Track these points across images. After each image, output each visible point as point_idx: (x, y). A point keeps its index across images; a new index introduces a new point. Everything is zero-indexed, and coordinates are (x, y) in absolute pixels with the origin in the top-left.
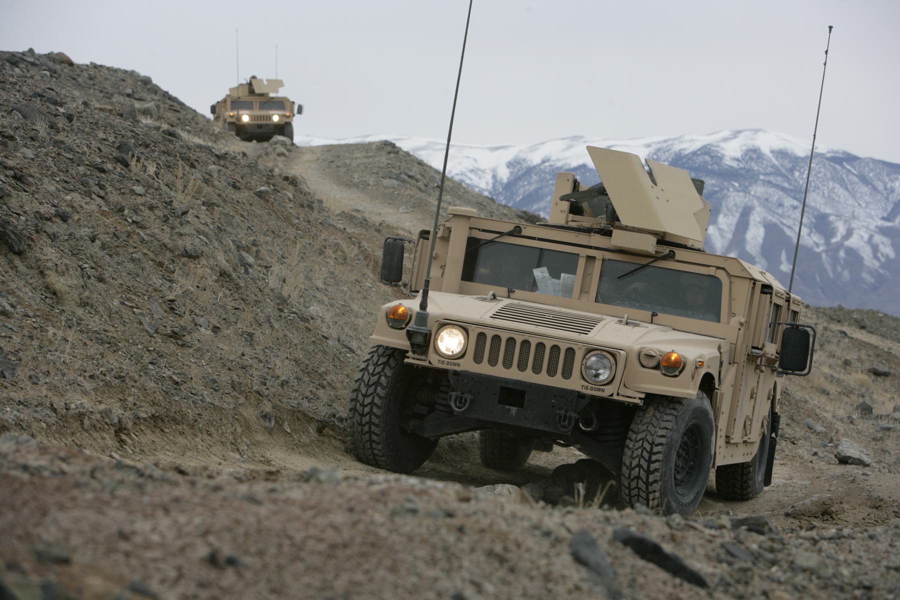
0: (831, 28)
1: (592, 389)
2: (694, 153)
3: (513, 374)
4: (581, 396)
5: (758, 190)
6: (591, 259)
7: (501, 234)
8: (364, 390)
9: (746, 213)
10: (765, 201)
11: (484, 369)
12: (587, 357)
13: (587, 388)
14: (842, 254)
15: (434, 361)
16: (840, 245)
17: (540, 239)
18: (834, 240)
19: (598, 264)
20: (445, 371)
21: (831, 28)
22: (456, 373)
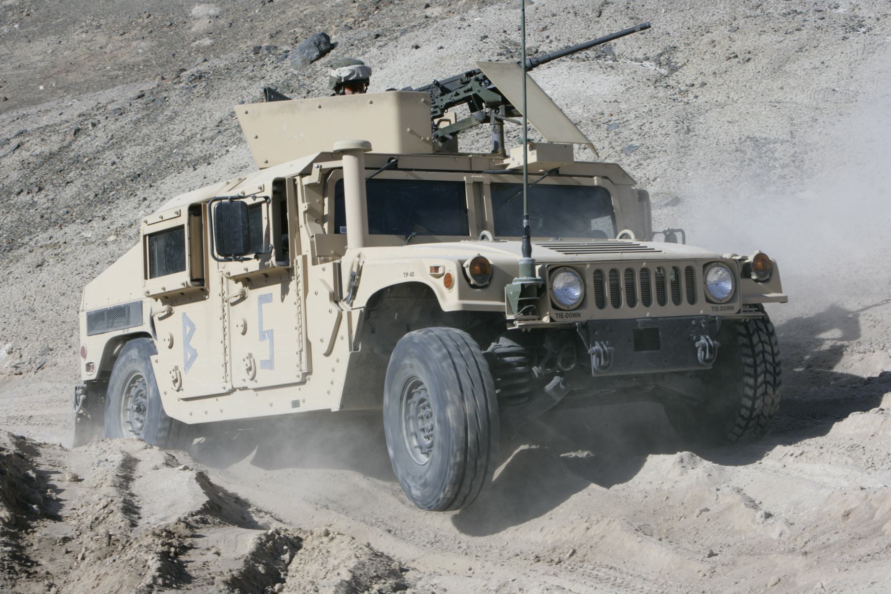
6: (478, 185)
19: (487, 190)
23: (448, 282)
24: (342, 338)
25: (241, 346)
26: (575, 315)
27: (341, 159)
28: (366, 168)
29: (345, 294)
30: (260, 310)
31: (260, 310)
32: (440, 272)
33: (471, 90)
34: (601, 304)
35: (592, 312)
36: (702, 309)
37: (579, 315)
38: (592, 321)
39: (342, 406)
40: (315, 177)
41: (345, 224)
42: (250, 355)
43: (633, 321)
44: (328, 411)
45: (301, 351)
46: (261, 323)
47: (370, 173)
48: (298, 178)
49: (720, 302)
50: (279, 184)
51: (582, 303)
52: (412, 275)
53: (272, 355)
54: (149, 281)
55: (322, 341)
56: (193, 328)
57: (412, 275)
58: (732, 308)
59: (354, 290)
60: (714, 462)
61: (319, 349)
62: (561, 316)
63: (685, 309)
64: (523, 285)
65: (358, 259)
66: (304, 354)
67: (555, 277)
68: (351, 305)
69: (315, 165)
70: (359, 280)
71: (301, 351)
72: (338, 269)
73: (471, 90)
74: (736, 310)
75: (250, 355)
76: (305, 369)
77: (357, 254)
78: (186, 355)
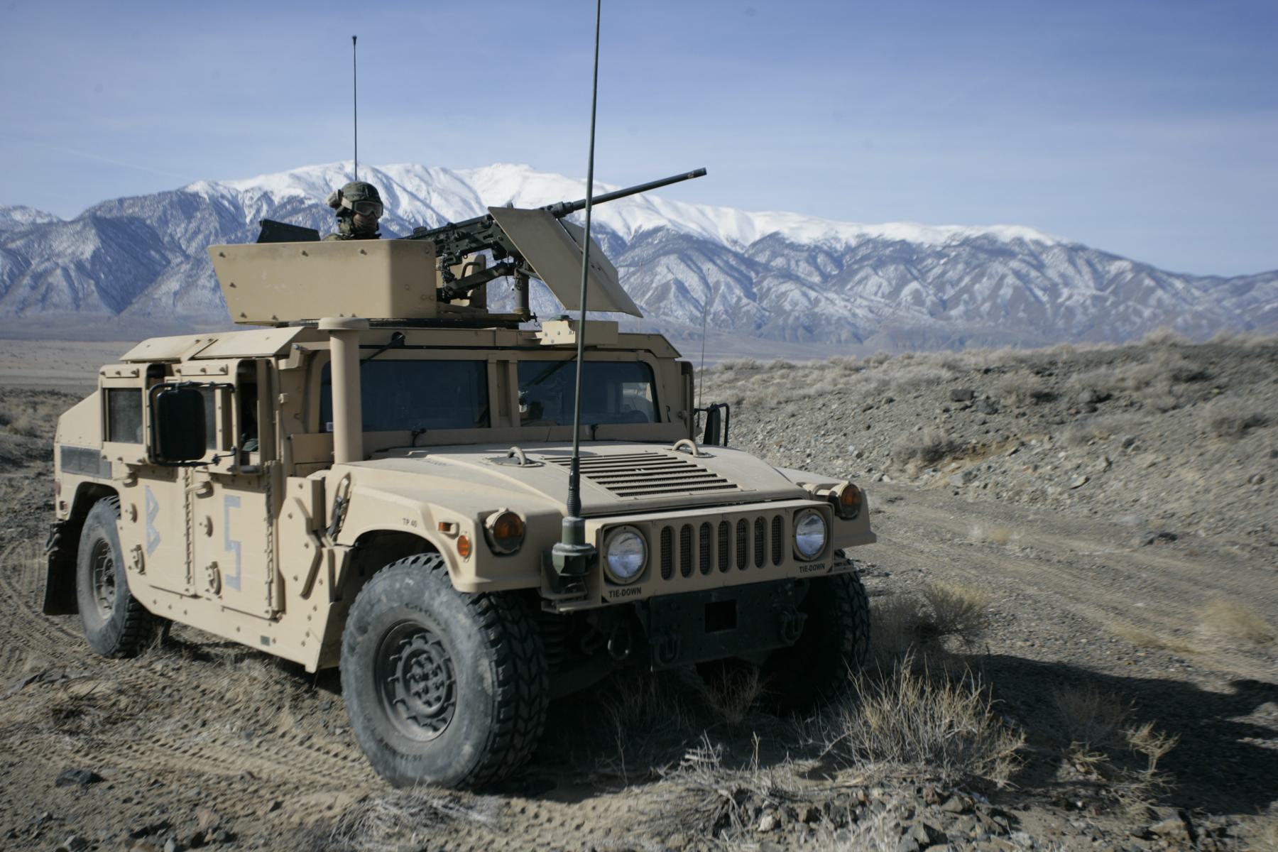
0: (355, 38)
1: (812, 568)
2: (978, 238)
3: (715, 580)
4: (798, 583)
5: (1014, 264)
6: (504, 364)
7: (382, 348)
8: (524, 710)
9: (1003, 277)
10: (1017, 274)
11: (679, 584)
12: (629, 528)
13: (616, 594)
14: (1063, 309)
15: (604, 594)
16: (1062, 304)
17: (428, 347)
18: (1060, 300)
19: (513, 371)
20: (629, 607)
21: (355, 38)
22: (645, 604)
23: (464, 547)
24: (321, 582)
25: (207, 549)
26: (633, 591)
27: (328, 340)
28: (361, 347)
29: (329, 523)
30: (227, 513)
31: (227, 513)
32: (453, 531)
33: (491, 236)
34: (667, 573)
35: (656, 586)
36: (790, 569)
37: (639, 591)
38: (655, 598)
39: (319, 667)
40: (294, 361)
41: (331, 420)
42: (215, 565)
43: (707, 593)
44: (302, 667)
45: (271, 582)
46: (227, 529)
47: (368, 353)
48: (273, 360)
49: (809, 558)
50: (248, 365)
51: (643, 573)
52: (414, 524)
53: (239, 573)
54: (107, 444)
55: (296, 579)
56: (156, 509)
57: (414, 524)
58: (823, 566)
59: (338, 520)
60: (516, 164)
61: (294, 590)
62: (616, 594)
63: (770, 573)
64: (567, 558)
65: (345, 482)
66: (274, 587)
67: (611, 540)
68: (335, 539)
69: (294, 346)
70: (346, 509)
71: (271, 582)
72: (319, 489)
73: (491, 236)
74: (827, 568)
75: (215, 565)
76: (275, 606)
77: (345, 473)
78: (149, 535)
